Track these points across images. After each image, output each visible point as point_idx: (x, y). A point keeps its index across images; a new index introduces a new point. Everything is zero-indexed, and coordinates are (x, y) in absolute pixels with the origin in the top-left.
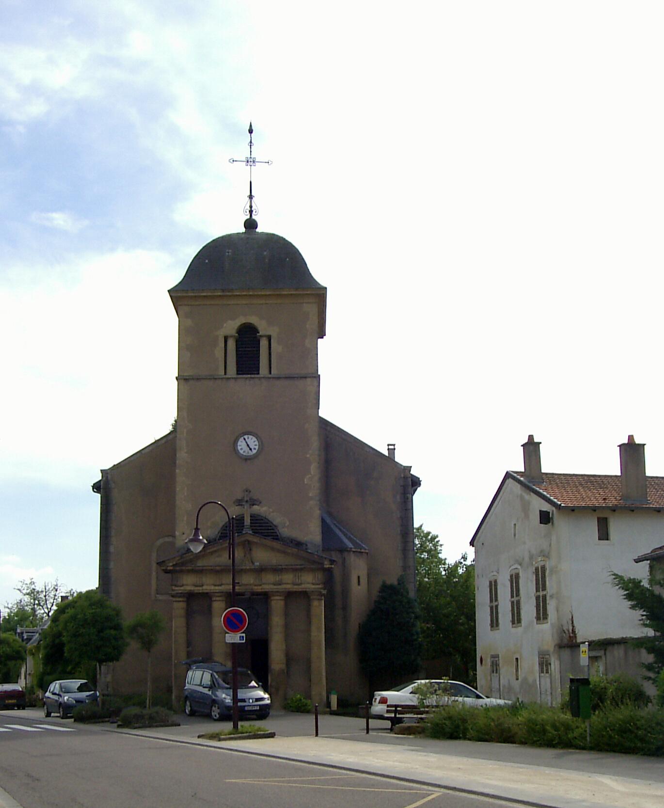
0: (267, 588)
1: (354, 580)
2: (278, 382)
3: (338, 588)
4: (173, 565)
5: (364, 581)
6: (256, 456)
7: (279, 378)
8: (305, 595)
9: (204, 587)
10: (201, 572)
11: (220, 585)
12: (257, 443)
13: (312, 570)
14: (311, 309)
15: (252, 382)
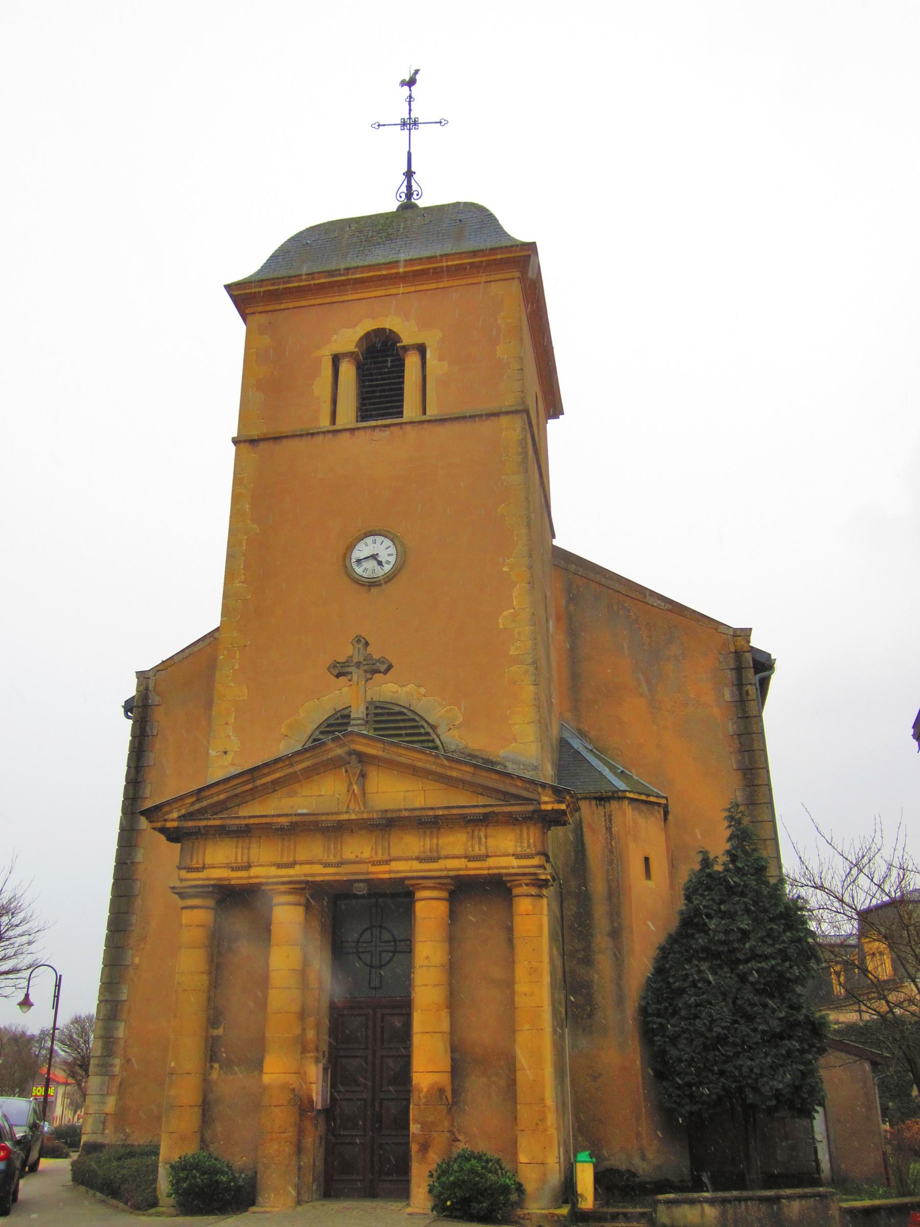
0: (402, 869)
1: (636, 868)
2: (439, 429)
3: (598, 886)
4: (179, 818)
5: (660, 866)
6: (390, 578)
7: (442, 421)
8: (496, 889)
9: (254, 871)
10: (244, 833)
11: (292, 865)
12: (393, 550)
13: (512, 821)
14: (506, 290)
15: (386, 434)
